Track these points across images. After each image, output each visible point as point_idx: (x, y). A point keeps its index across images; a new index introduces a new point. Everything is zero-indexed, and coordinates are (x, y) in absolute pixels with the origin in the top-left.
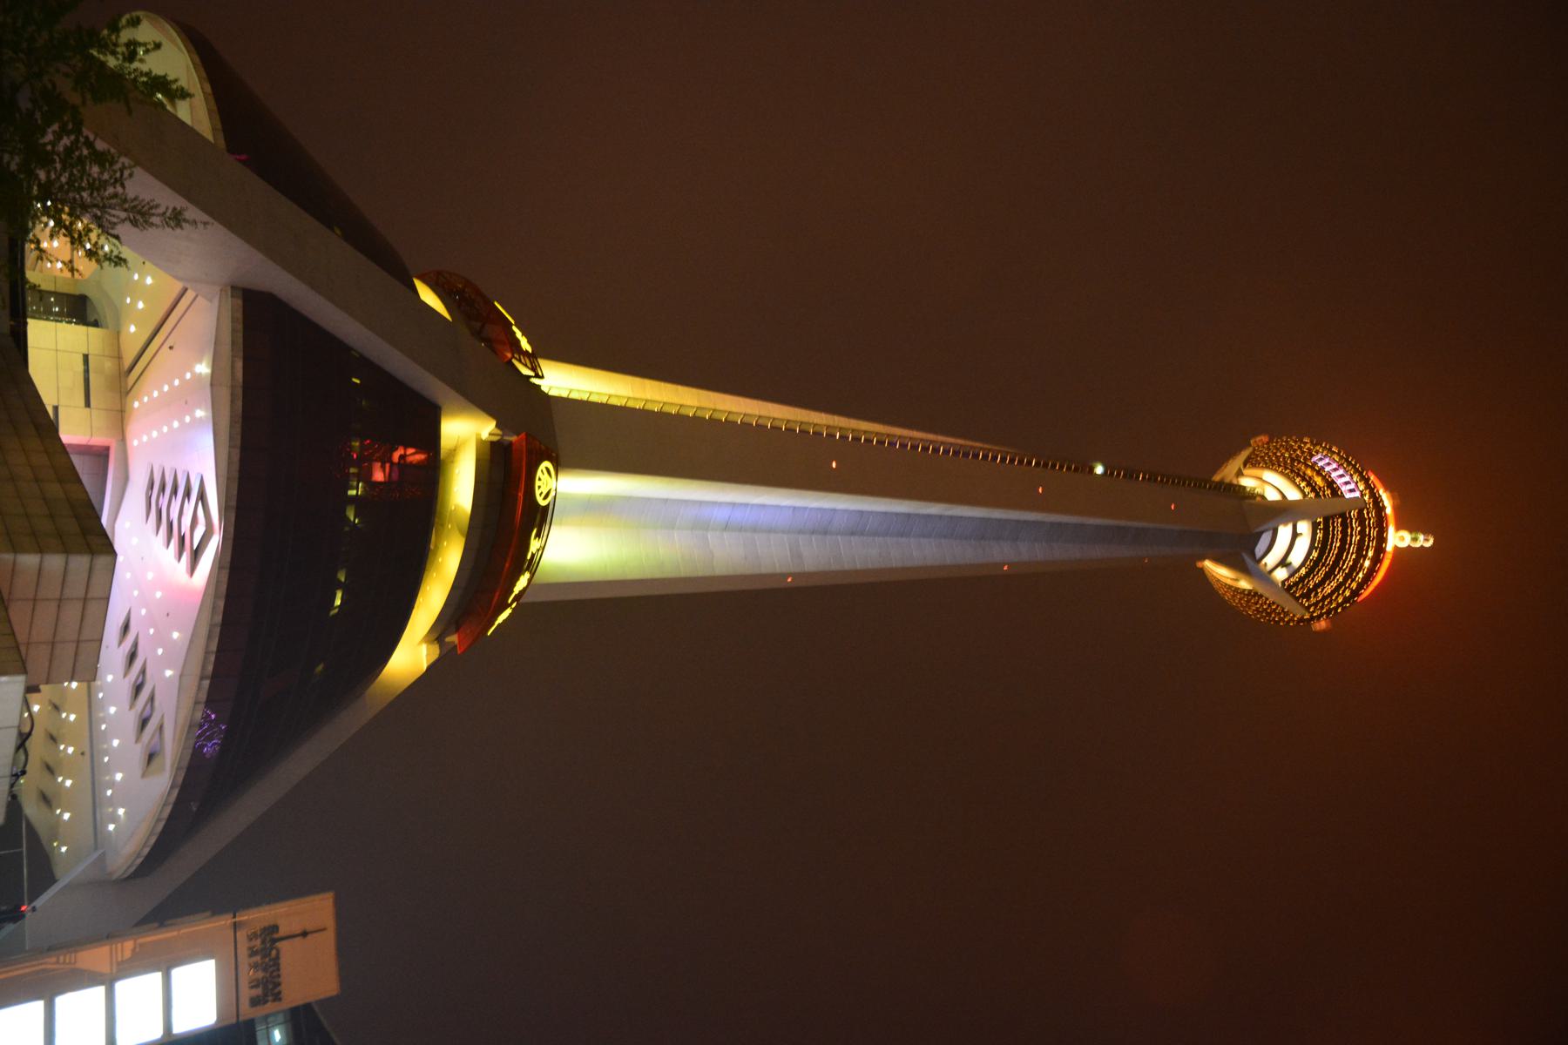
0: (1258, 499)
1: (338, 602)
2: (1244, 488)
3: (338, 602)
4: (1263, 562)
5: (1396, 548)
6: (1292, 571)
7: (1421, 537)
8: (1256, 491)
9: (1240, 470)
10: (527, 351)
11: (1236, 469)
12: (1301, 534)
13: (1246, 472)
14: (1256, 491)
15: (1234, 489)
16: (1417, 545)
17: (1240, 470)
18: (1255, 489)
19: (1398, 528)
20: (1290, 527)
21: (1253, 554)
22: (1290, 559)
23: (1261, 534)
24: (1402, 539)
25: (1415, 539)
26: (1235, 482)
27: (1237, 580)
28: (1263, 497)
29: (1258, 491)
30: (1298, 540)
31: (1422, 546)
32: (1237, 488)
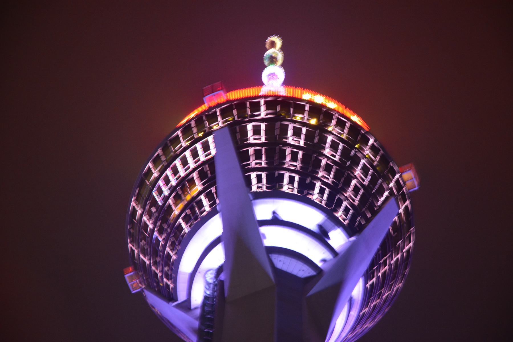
0: (222, 277)
1: (309, 143)
2: (206, 298)
3: (309, 143)
4: (320, 265)
5: (286, 83)
6: (330, 224)
7: (270, 52)
8: (211, 281)
9: (180, 306)
10: (209, 311)
11: (180, 313)
12: (274, 213)
13: (182, 296)
14: (211, 281)
15: (209, 313)
16: (280, 57)
17: (180, 306)
18: (208, 284)
19: (260, 84)
20: (263, 230)
21: (308, 280)
22: (312, 226)
23: (279, 273)
24: (272, 75)
25: (273, 60)
26: (198, 312)
27: (351, 301)
28: (220, 270)
29: (210, 277)
30: (284, 217)
31: (283, 65)
32: (207, 309)
